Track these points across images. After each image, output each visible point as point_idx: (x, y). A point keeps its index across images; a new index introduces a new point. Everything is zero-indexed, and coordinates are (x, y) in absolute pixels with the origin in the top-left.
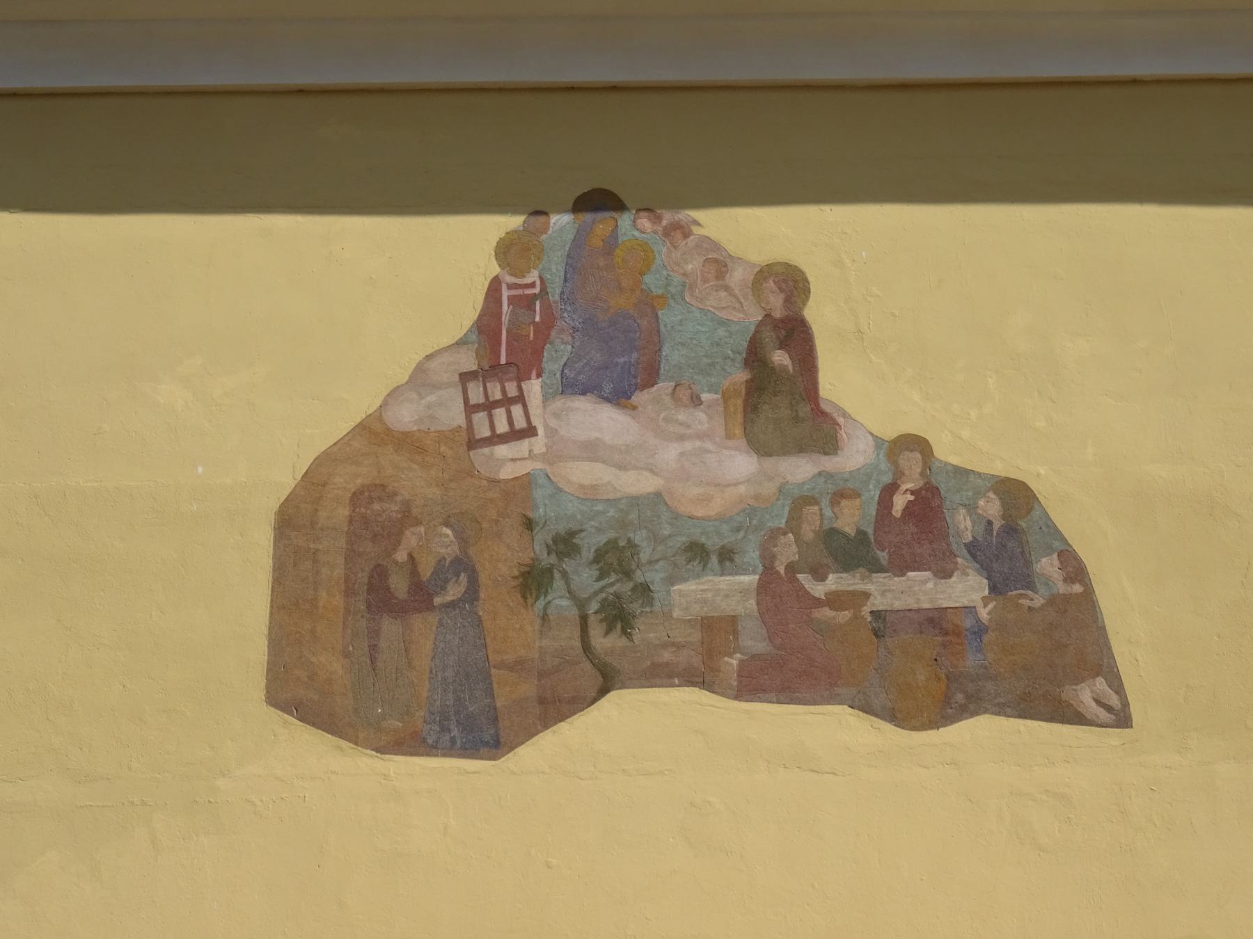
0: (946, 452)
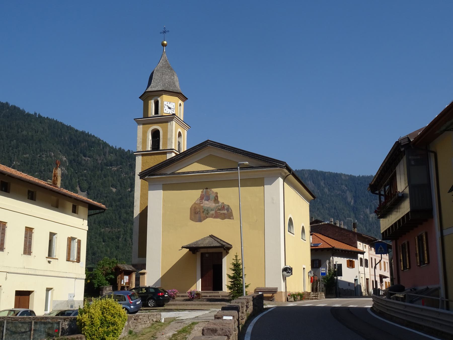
0: (225, 203)
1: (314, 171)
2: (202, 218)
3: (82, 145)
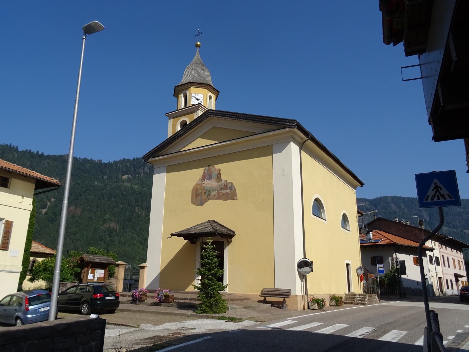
0: (228, 181)
1: (395, 197)
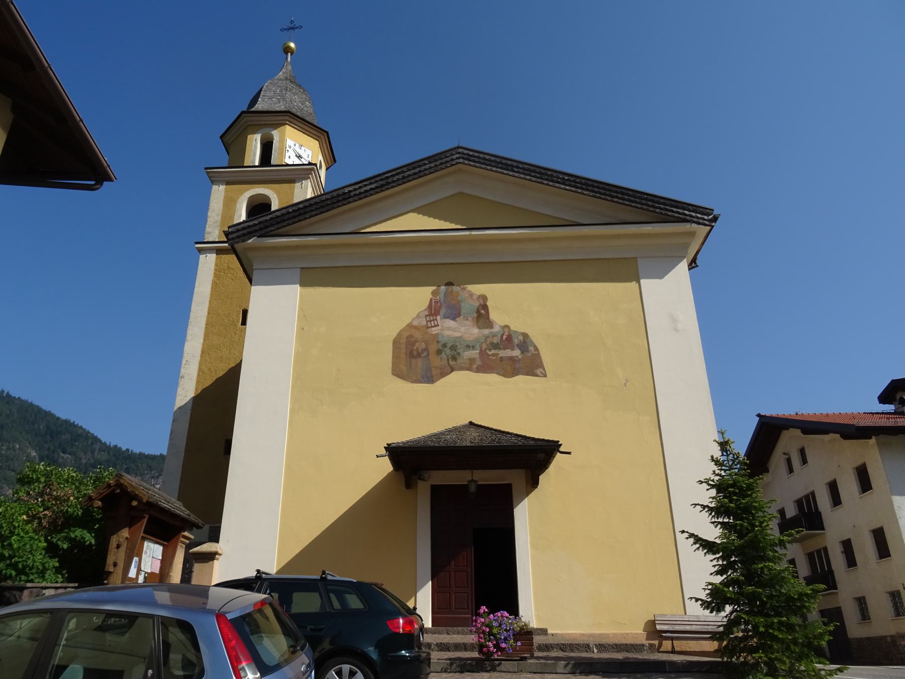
0: (513, 328)
2: (435, 372)
3: (63, 437)
